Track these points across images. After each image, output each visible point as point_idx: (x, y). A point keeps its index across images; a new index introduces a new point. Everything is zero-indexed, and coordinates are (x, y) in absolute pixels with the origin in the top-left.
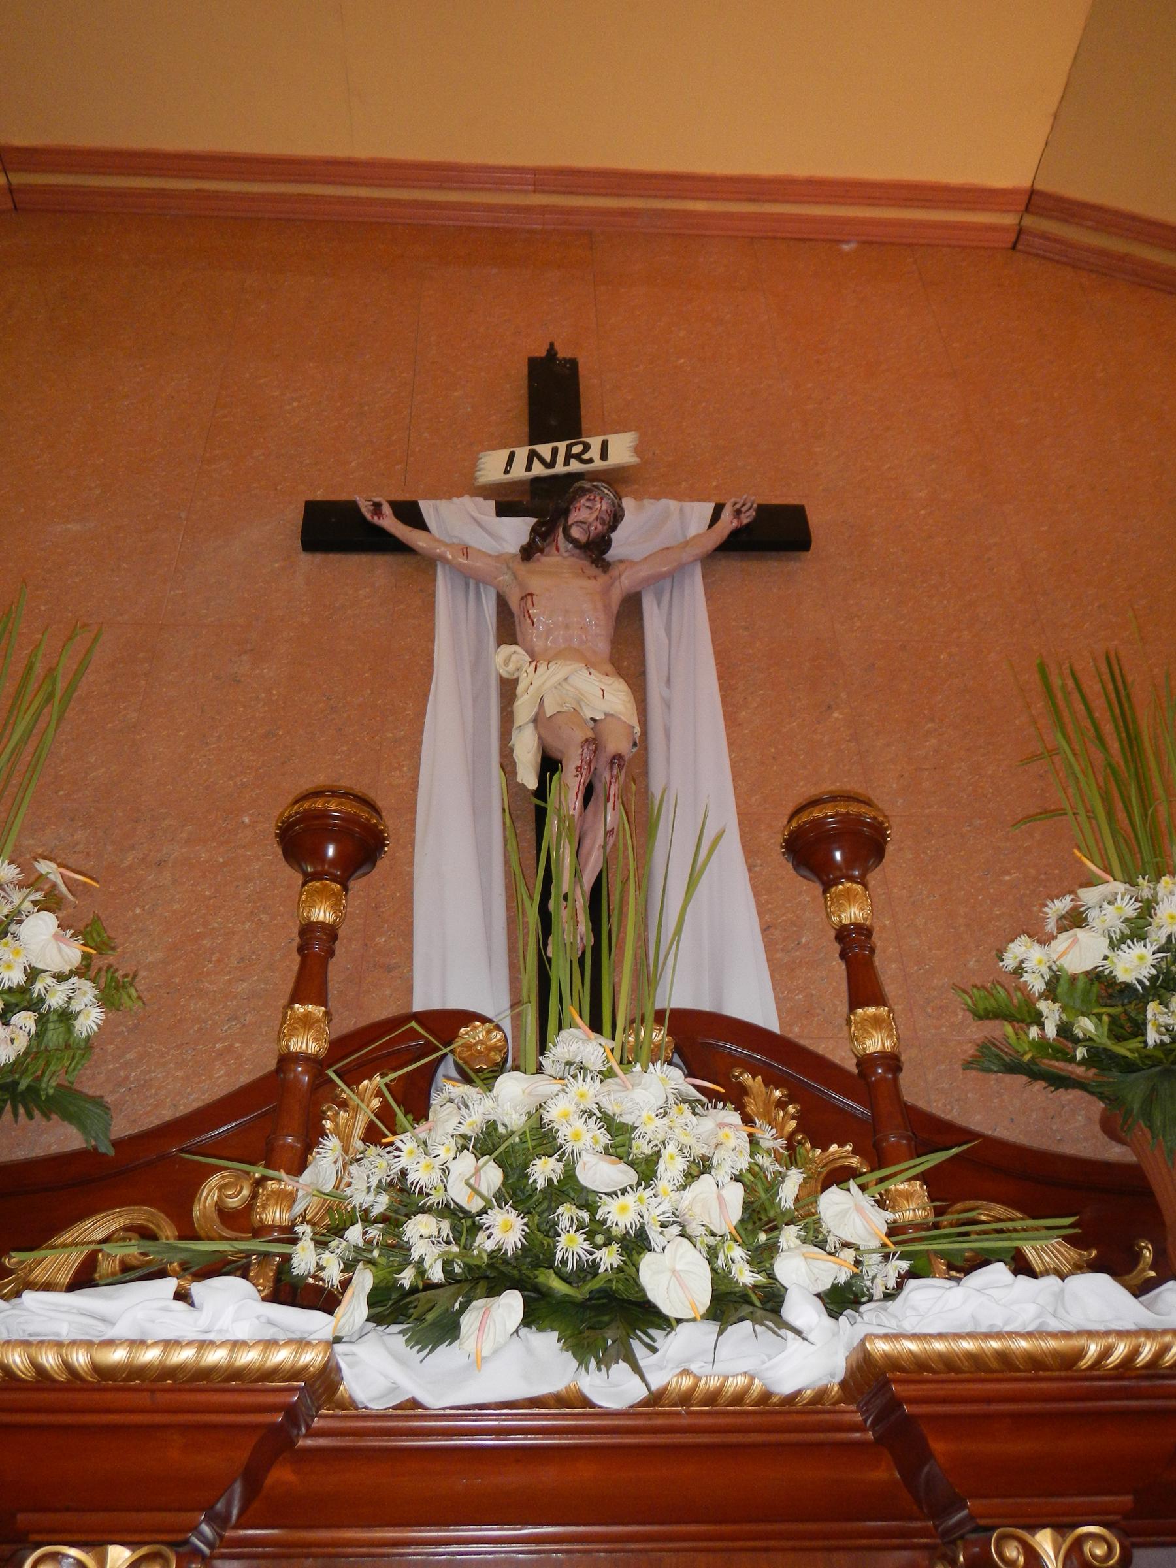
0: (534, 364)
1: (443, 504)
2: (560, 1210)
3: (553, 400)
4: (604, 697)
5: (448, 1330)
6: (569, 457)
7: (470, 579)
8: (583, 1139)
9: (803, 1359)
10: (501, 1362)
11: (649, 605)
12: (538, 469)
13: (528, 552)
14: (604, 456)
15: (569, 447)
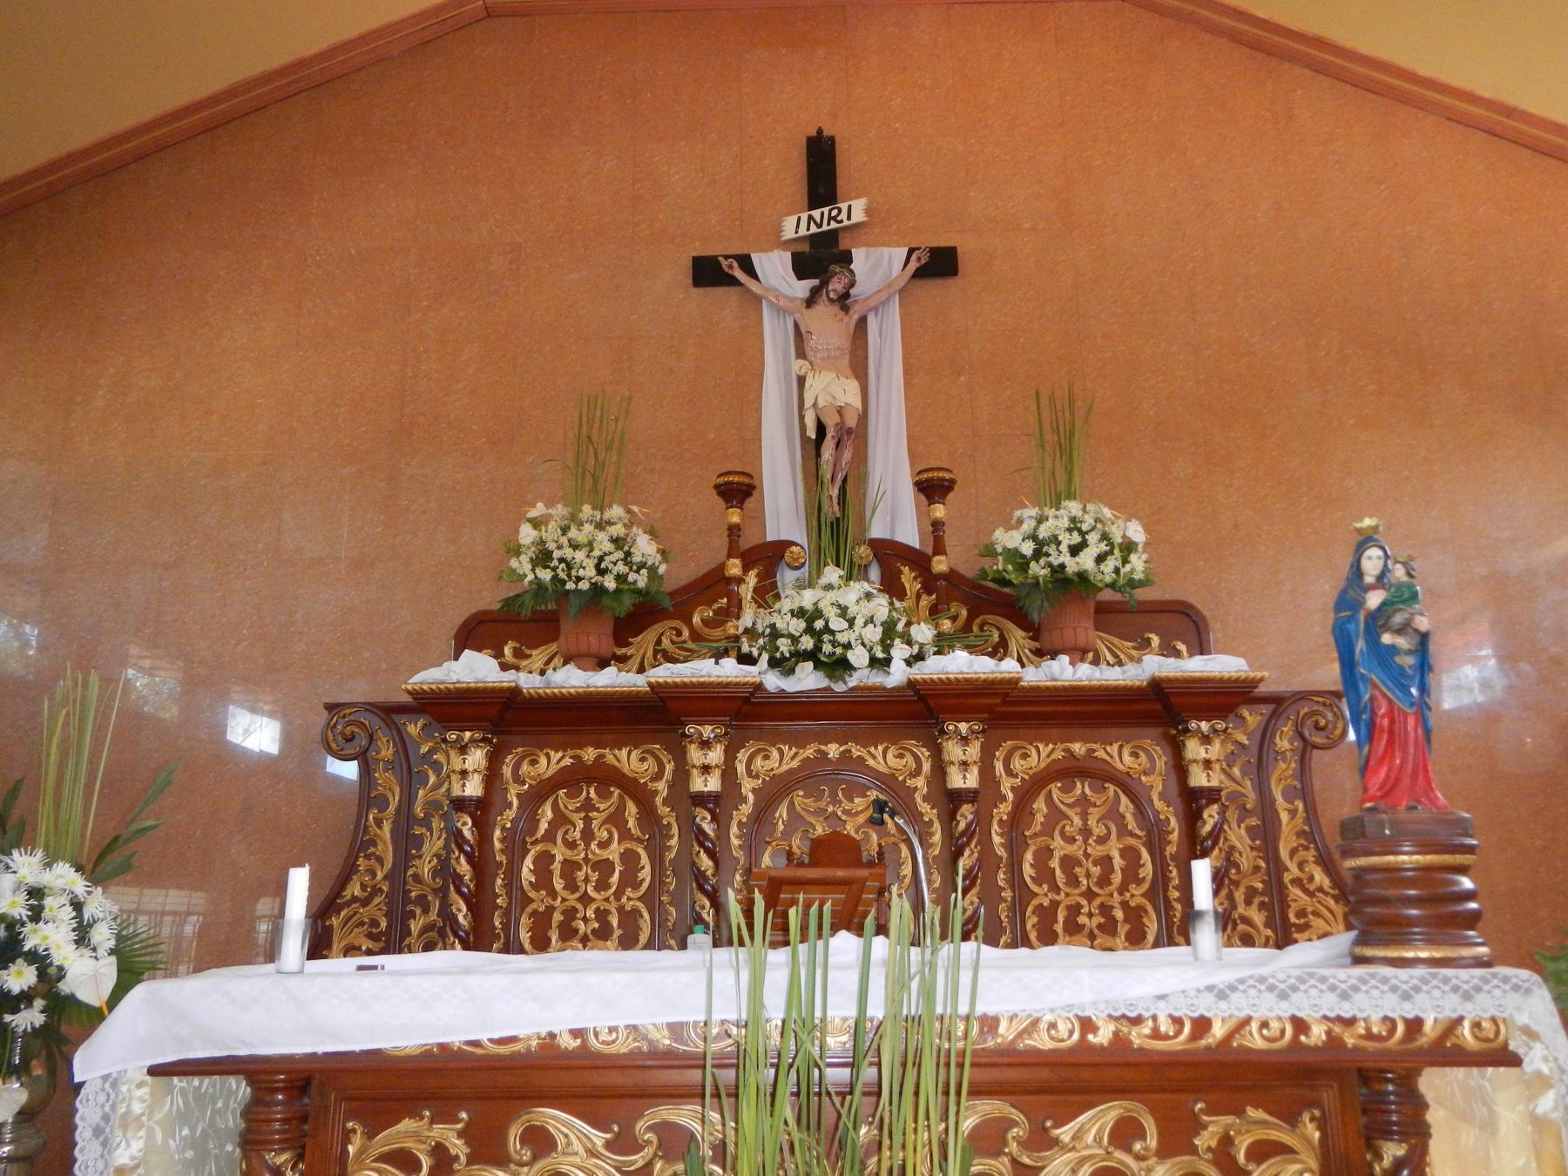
0: (810, 141)
1: (762, 255)
3: (821, 173)
4: (847, 392)
5: (791, 671)
6: (830, 218)
7: (780, 311)
9: (898, 674)
10: (807, 679)
11: (872, 322)
13: (810, 302)
14: (849, 218)
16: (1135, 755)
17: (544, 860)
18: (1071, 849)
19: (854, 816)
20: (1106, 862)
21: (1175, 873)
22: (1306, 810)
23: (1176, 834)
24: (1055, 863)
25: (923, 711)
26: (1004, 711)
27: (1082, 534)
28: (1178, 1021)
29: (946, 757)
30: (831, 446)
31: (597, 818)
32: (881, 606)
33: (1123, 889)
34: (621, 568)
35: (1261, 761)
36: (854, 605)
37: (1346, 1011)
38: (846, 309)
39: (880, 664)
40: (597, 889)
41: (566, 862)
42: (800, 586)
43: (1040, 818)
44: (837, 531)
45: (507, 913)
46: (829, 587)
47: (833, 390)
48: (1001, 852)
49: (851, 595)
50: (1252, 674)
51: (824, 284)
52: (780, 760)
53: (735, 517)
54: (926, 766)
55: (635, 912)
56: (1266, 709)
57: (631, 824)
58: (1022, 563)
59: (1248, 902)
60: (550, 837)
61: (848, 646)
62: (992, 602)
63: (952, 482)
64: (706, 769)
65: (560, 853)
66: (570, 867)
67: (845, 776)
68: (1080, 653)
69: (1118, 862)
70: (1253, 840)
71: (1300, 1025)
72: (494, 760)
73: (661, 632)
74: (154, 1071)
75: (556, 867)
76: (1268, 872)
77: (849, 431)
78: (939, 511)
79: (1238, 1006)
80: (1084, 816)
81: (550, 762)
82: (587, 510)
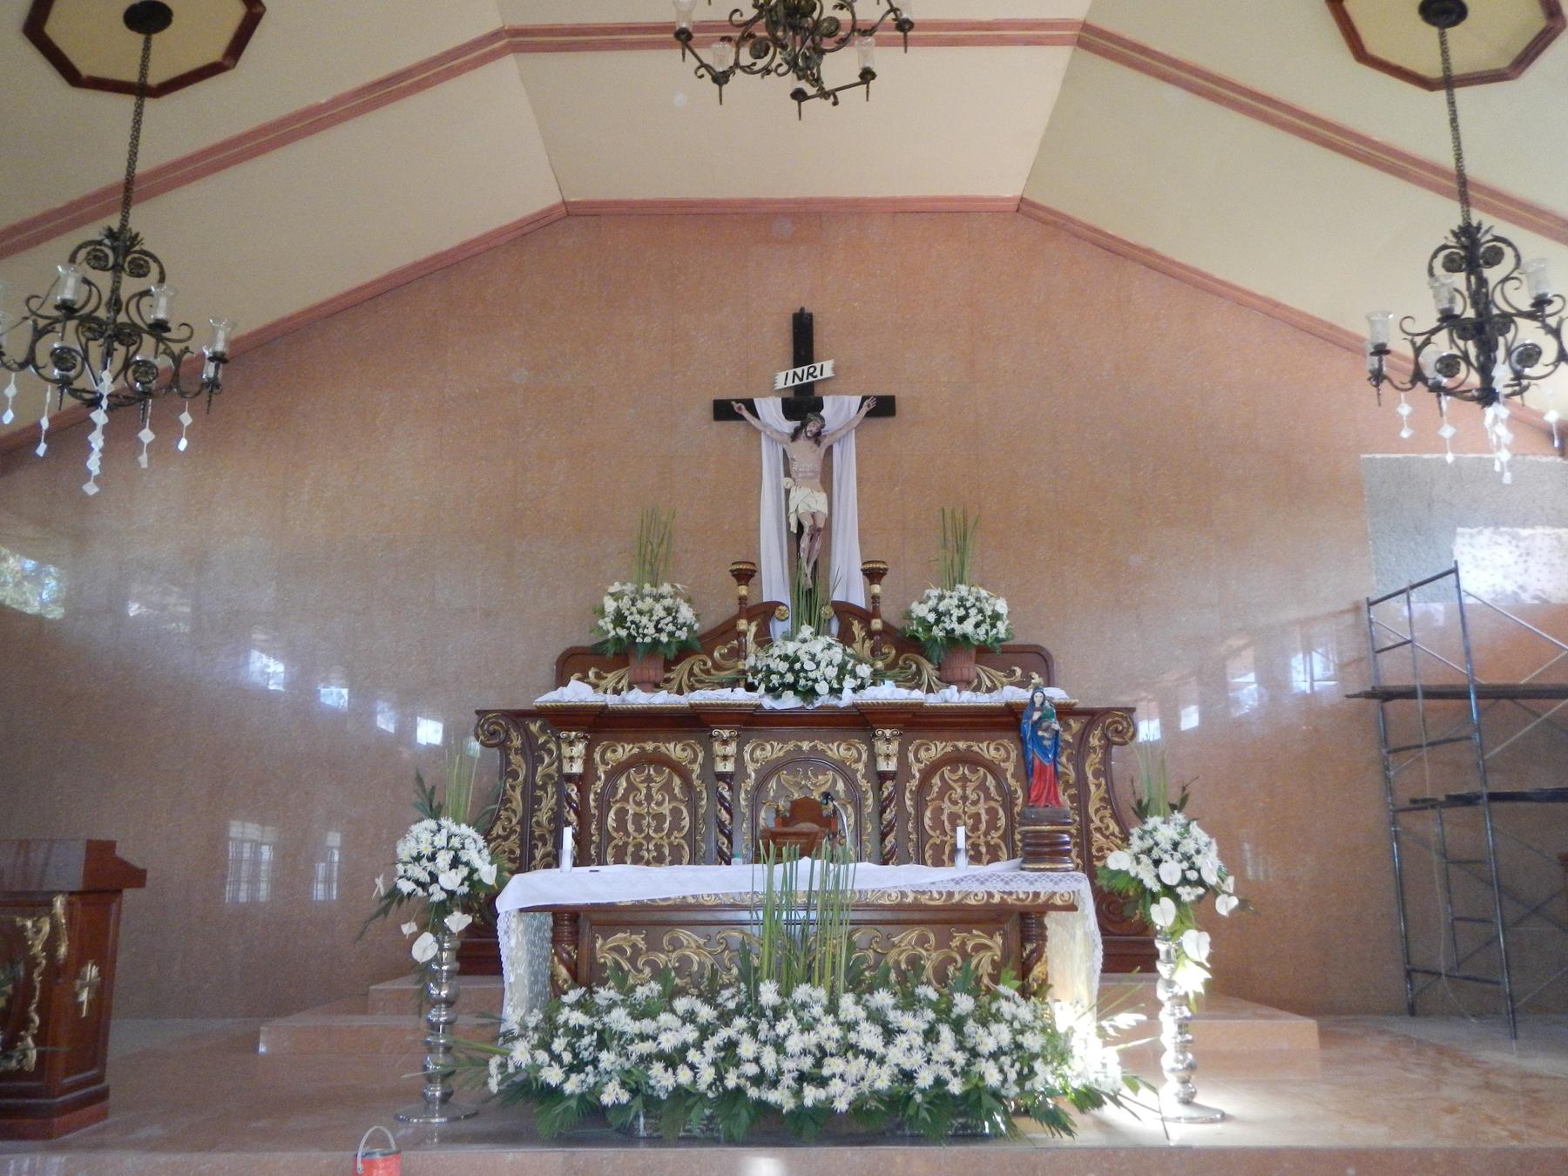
4: (819, 503)
7: (772, 440)
8: (805, 658)
9: (847, 698)
10: (789, 701)
11: (836, 450)
12: (797, 382)
13: (795, 436)
16: (997, 749)
17: (622, 813)
18: (955, 809)
19: (819, 784)
20: (977, 817)
24: (945, 817)
25: (863, 721)
26: (913, 721)
27: (966, 609)
28: (940, 893)
30: (806, 540)
31: (655, 787)
32: (837, 654)
33: (986, 834)
34: (671, 628)
36: (819, 651)
37: (1007, 889)
38: (818, 442)
39: (835, 692)
40: (655, 831)
41: (635, 815)
42: (789, 637)
43: (936, 789)
44: (810, 599)
45: (598, 847)
46: (804, 641)
47: (809, 501)
48: (911, 810)
49: (817, 646)
51: (804, 426)
52: (773, 750)
53: (743, 590)
54: (864, 756)
55: (680, 846)
56: (1084, 720)
57: (677, 791)
58: (929, 628)
60: (625, 798)
62: (906, 647)
63: (885, 570)
64: (725, 758)
65: (631, 809)
66: (638, 817)
67: (815, 762)
68: (964, 684)
69: (984, 817)
71: (990, 895)
72: (589, 750)
73: (695, 663)
74: (522, 910)
75: (629, 818)
77: (819, 530)
78: (877, 589)
79: (965, 887)
80: (964, 788)
81: (624, 751)
82: (647, 588)
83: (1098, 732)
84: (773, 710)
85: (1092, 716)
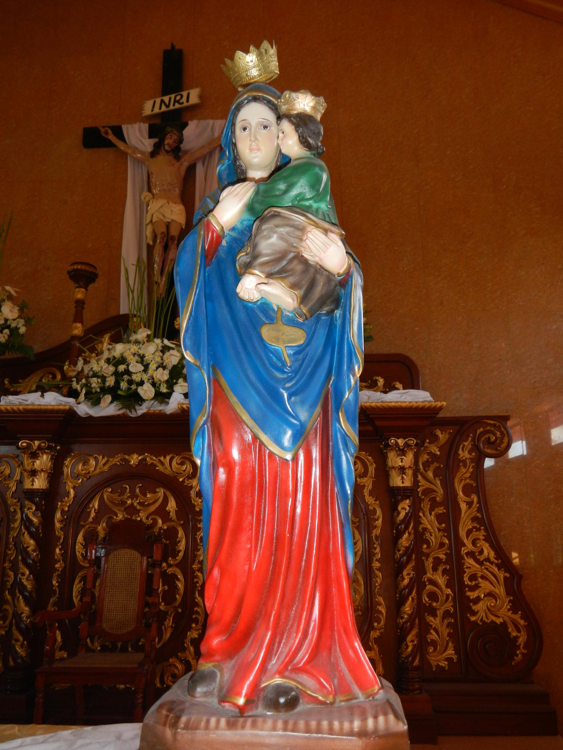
1: (130, 126)
2: (124, 376)
6: (175, 101)
7: (138, 162)
10: (108, 408)
11: (200, 169)
12: (164, 108)
13: (153, 154)
14: (188, 101)
15: (175, 97)
21: (378, 550)
22: (479, 502)
23: (380, 520)
29: (390, 464)
35: (447, 465)
39: (163, 397)
50: (434, 404)
53: (80, 294)
59: (435, 569)
61: (141, 383)
70: (440, 524)
76: (450, 548)
83: (468, 444)
84: (90, 418)
85: (462, 426)
